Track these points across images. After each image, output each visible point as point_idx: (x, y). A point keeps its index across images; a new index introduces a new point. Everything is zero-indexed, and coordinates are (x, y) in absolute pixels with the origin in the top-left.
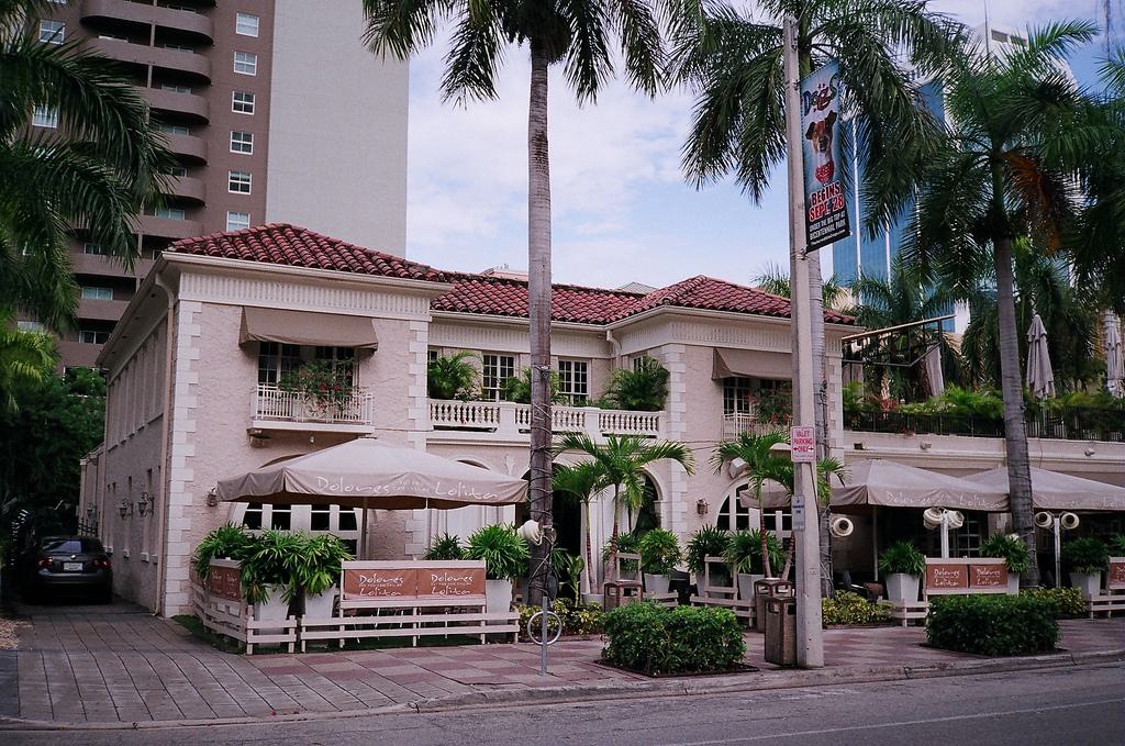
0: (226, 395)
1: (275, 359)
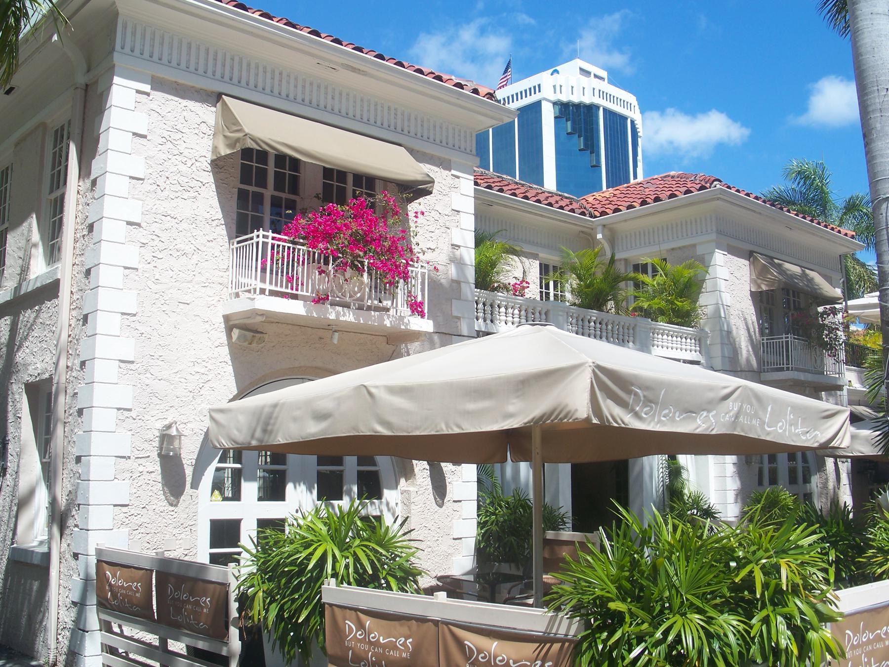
0: (189, 249)
1: (267, 192)
